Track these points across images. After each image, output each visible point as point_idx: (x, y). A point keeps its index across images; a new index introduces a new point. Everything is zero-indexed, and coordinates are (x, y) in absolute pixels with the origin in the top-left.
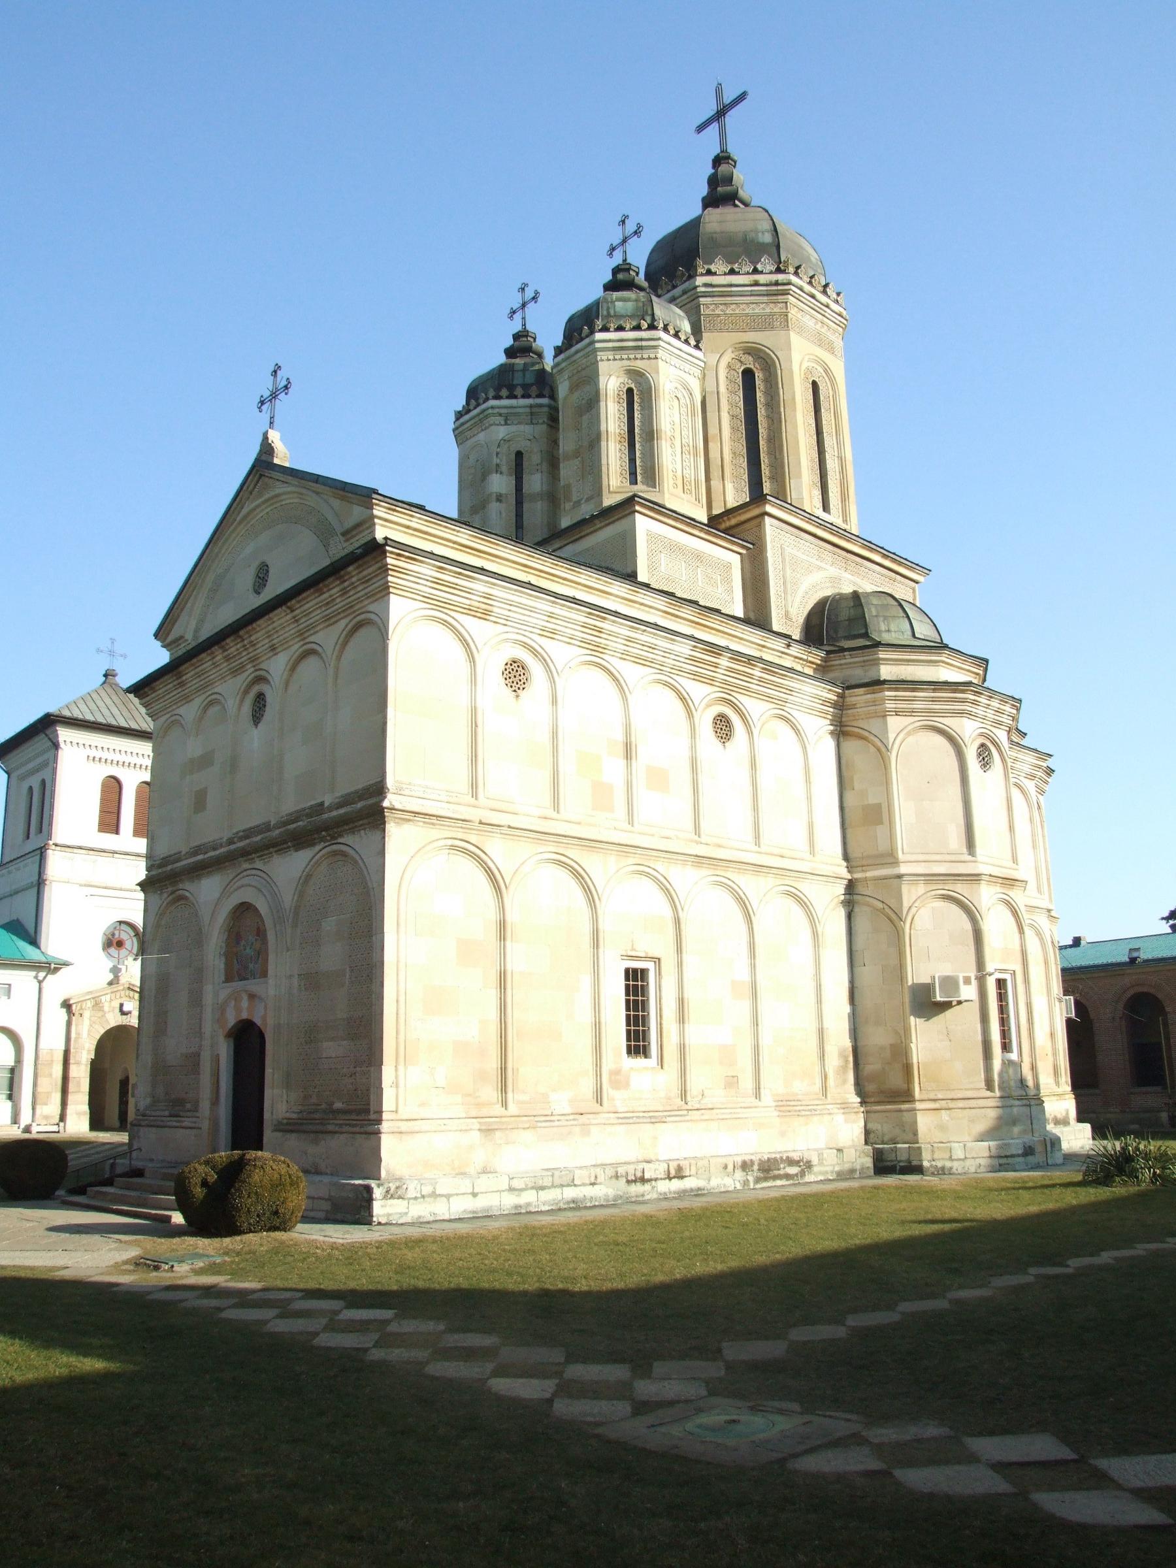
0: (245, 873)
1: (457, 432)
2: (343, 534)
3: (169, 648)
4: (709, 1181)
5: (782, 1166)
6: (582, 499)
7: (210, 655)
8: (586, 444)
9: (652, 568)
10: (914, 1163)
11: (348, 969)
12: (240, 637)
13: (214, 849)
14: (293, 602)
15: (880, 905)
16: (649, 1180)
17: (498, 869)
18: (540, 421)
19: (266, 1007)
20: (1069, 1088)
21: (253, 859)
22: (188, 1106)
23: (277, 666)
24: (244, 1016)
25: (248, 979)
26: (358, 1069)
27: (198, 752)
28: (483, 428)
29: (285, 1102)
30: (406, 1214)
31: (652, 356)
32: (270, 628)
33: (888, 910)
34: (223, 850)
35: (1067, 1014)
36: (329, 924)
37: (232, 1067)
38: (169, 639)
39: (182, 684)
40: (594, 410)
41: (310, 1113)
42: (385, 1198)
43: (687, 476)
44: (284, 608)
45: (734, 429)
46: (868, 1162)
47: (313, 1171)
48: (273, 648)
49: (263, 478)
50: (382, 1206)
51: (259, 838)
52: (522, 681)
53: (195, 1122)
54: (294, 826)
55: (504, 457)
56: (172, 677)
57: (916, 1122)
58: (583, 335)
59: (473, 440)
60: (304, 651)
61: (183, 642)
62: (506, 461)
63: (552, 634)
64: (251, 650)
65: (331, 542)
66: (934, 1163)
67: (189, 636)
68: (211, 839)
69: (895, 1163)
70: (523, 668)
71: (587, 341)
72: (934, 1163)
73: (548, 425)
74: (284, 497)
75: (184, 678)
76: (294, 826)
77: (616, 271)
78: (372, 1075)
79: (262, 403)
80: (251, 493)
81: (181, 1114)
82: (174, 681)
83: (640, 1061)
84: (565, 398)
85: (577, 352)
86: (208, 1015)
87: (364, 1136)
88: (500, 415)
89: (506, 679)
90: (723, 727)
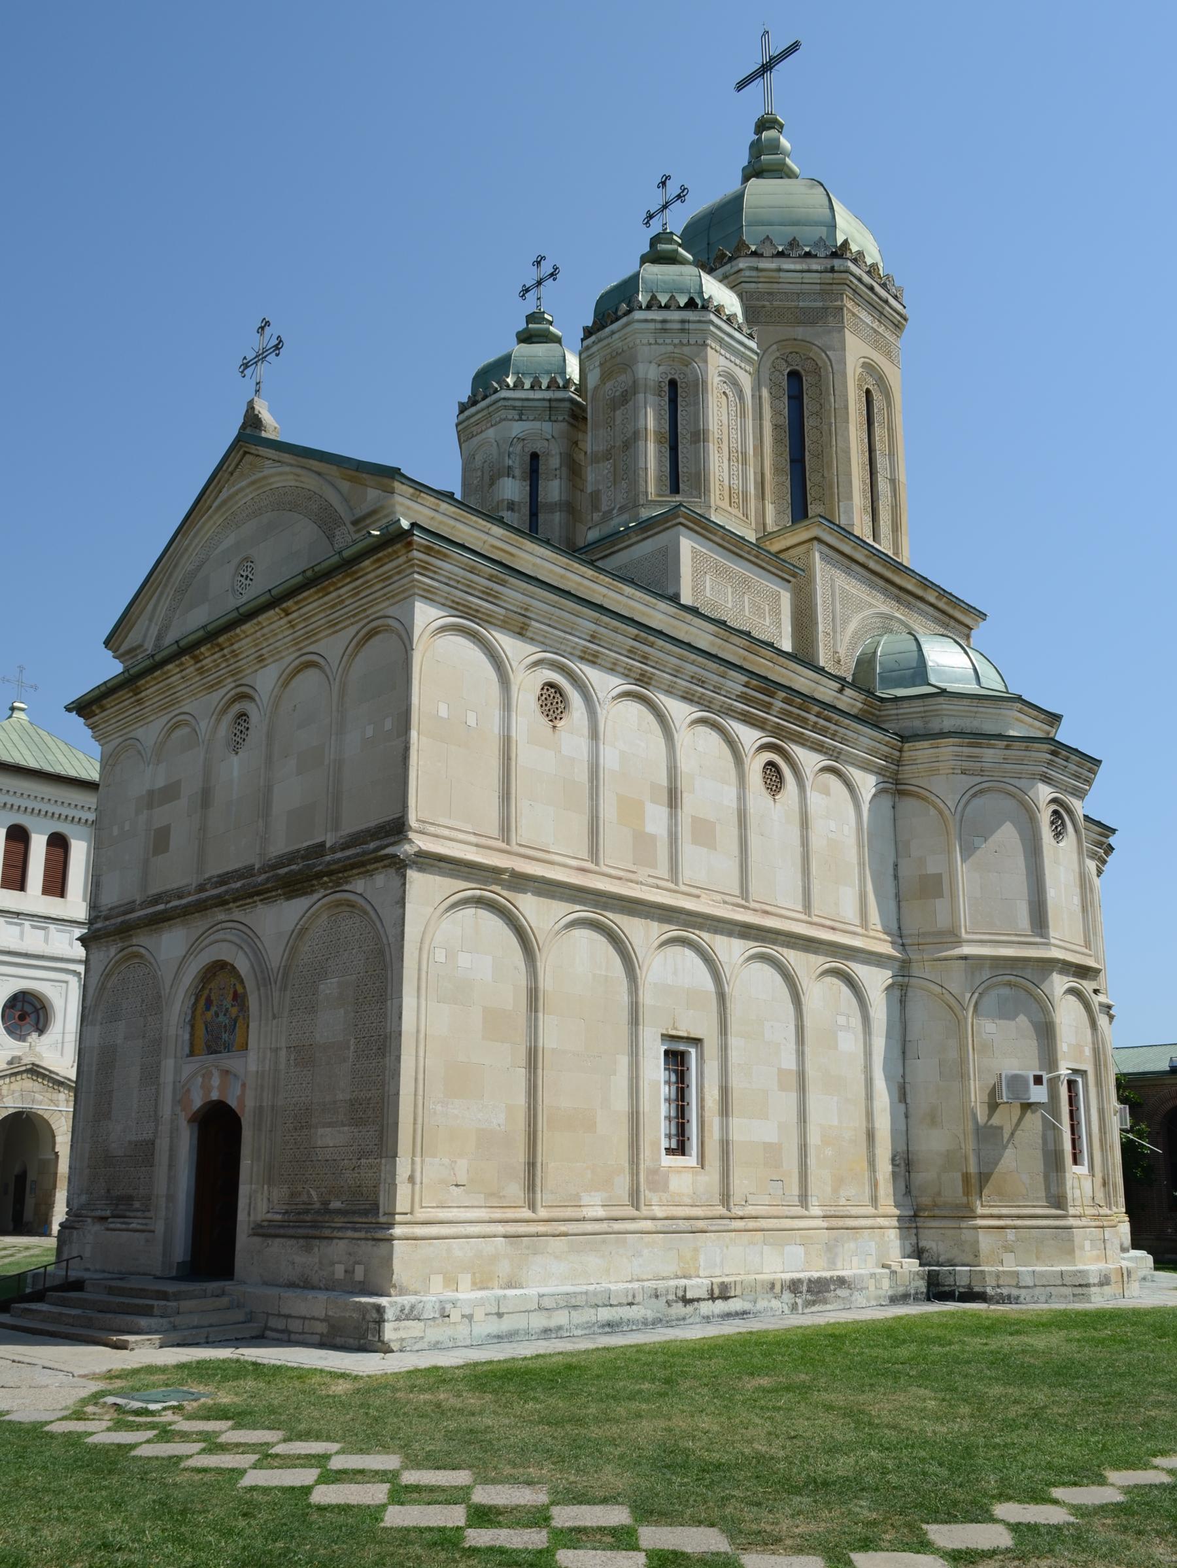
0: (219, 926)
1: (460, 427)
2: (355, 523)
3: (122, 659)
4: (755, 1303)
5: (832, 1287)
6: (613, 509)
7: (177, 666)
8: (619, 443)
9: (697, 589)
10: (976, 1289)
11: (353, 1040)
12: (218, 645)
13: (180, 897)
14: (290, 603)
15: (938, 989)
16: (691, 1301)
17: (530, 927)
18: (560, 418)
19: (244, 1085)
20: (1124, 1210)
21: (230, 909)
22: (137, 1205)
23: (265, 681)
24: (215, 1096)
25: (220, 1052)
26: (363, 1161)
27: (160, 783)
28: (493, 423)
29: (265, 1200)
30: (422, 1338)
31: (700, 342)
32: (259, 634)
33: (947, 996)
34: (190, 899)
35: (1121, 1125)
36: (329, 987)
37: (195, 1157)
38: (122, 650)
39: (139, 702)
40: (631, 403)
41: (299, 1213)
42: (398, 1319)
43: (735, 487)
44: (277, 610)
45: (777, 441)
46: (922, 1285)
47: (302, 1284)
48: (261, 659)
49: (247, 456)
50: (395, 1329)
51: (239, 884)
52: (560, 710)
53: (146, 1224)
54: (286, 870)
55: (518, 458)
56: (128, 693)
57: (977, 1242)
58: (620, 313)
59: (479, 438)
60: (302, 664)
61: (142, 652)
62: (518, 464)
63: (592, 659)
64: (232, 661)
65: (337, 533)
66: (999, 1290)
67: (149, 646)
68: (175, 886)
69: (953, 1288)
70: (561, 695)
71: (624, 320)
72: (999, 1290)
73: (569, 423)
74: (272, 480)
75: (143, 694)
76: (286, 870)
77: (655, 241)
78: (383, 1168)
79: (246, 366)
80: (232, 474)
81: (128, 1214)
82: (131, 697)
83: (678, 1161)
84: (596, 388)
85: (613, 333)
86: (167, 1095)
87: (370, 1243)
88: (514, 408)
89: (542, 706)
90: (773, 777)
